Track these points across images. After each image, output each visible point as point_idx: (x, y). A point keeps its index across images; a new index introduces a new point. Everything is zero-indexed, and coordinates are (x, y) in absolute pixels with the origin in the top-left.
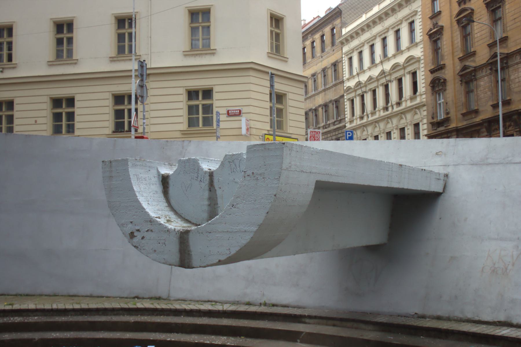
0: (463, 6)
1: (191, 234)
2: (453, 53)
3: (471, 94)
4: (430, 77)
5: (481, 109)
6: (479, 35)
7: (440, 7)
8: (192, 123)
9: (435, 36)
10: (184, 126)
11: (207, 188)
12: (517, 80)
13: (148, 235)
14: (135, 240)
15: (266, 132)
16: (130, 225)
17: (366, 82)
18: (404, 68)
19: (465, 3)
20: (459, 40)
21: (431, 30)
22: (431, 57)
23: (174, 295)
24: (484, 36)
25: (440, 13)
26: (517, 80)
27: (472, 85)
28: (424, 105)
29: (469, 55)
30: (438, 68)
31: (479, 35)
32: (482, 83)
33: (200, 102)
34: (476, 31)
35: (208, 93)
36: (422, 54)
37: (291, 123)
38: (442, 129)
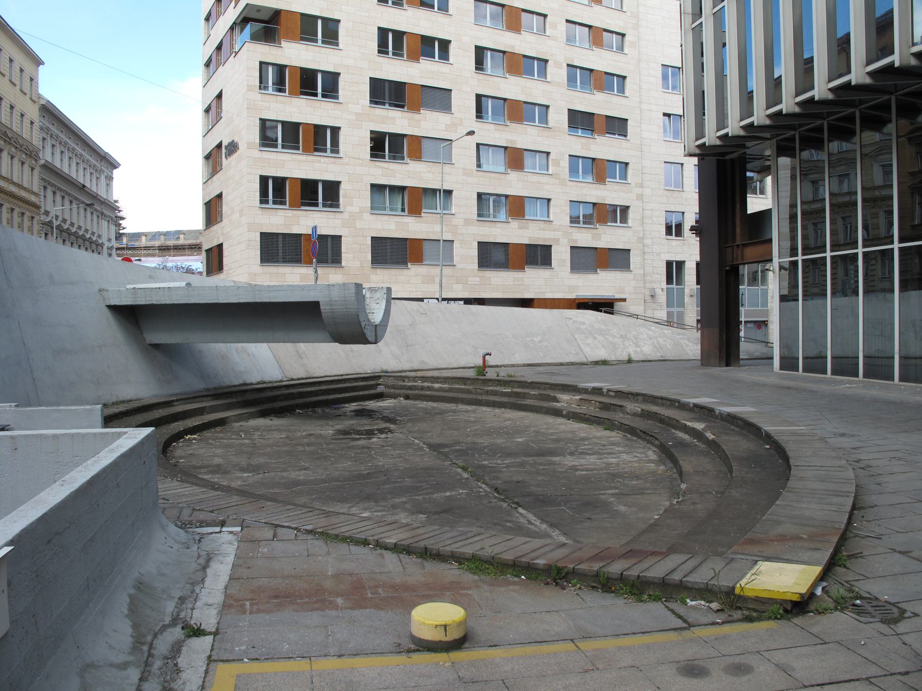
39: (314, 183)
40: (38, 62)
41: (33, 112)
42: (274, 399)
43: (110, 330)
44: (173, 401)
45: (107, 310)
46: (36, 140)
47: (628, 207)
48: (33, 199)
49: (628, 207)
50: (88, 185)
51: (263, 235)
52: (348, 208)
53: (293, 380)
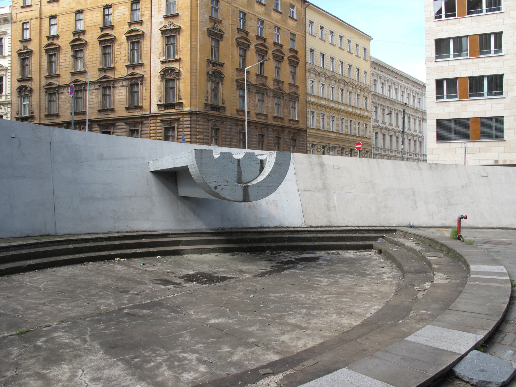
1: (249, 187)
2: (40, 71)
3: (52, 103)
4: (17, 85)
5: (61, 114)
6: (63, 64)
7: (30, 36)
9: (24, 56)
11: (237, 166)
13: (225, 188)
19: (53, 40)
20: (46, 63)
21: (21, 50)
22: (19, 70)
24: (67, 66)
25: (30, 40)
27: (54, 98)
28: (9, 104)
29: (51, 76)
30: (24, 79)
31: (63, 64)
32: (63, 97)
34: (61, 61)
36: (10, 65)
39: (480, 79)
40: (369, 38)
41: (366, 66)
42: (246, 241)
43: (154, 186)
44: (169, 234)
45: (151, 174)
46: (370, 81)
47: (501, 33)
48: (366, 114)
49: (501, 33)
50: (411, 103)
51: (438, 121)
52: (510, 94)
53: (311, 227)
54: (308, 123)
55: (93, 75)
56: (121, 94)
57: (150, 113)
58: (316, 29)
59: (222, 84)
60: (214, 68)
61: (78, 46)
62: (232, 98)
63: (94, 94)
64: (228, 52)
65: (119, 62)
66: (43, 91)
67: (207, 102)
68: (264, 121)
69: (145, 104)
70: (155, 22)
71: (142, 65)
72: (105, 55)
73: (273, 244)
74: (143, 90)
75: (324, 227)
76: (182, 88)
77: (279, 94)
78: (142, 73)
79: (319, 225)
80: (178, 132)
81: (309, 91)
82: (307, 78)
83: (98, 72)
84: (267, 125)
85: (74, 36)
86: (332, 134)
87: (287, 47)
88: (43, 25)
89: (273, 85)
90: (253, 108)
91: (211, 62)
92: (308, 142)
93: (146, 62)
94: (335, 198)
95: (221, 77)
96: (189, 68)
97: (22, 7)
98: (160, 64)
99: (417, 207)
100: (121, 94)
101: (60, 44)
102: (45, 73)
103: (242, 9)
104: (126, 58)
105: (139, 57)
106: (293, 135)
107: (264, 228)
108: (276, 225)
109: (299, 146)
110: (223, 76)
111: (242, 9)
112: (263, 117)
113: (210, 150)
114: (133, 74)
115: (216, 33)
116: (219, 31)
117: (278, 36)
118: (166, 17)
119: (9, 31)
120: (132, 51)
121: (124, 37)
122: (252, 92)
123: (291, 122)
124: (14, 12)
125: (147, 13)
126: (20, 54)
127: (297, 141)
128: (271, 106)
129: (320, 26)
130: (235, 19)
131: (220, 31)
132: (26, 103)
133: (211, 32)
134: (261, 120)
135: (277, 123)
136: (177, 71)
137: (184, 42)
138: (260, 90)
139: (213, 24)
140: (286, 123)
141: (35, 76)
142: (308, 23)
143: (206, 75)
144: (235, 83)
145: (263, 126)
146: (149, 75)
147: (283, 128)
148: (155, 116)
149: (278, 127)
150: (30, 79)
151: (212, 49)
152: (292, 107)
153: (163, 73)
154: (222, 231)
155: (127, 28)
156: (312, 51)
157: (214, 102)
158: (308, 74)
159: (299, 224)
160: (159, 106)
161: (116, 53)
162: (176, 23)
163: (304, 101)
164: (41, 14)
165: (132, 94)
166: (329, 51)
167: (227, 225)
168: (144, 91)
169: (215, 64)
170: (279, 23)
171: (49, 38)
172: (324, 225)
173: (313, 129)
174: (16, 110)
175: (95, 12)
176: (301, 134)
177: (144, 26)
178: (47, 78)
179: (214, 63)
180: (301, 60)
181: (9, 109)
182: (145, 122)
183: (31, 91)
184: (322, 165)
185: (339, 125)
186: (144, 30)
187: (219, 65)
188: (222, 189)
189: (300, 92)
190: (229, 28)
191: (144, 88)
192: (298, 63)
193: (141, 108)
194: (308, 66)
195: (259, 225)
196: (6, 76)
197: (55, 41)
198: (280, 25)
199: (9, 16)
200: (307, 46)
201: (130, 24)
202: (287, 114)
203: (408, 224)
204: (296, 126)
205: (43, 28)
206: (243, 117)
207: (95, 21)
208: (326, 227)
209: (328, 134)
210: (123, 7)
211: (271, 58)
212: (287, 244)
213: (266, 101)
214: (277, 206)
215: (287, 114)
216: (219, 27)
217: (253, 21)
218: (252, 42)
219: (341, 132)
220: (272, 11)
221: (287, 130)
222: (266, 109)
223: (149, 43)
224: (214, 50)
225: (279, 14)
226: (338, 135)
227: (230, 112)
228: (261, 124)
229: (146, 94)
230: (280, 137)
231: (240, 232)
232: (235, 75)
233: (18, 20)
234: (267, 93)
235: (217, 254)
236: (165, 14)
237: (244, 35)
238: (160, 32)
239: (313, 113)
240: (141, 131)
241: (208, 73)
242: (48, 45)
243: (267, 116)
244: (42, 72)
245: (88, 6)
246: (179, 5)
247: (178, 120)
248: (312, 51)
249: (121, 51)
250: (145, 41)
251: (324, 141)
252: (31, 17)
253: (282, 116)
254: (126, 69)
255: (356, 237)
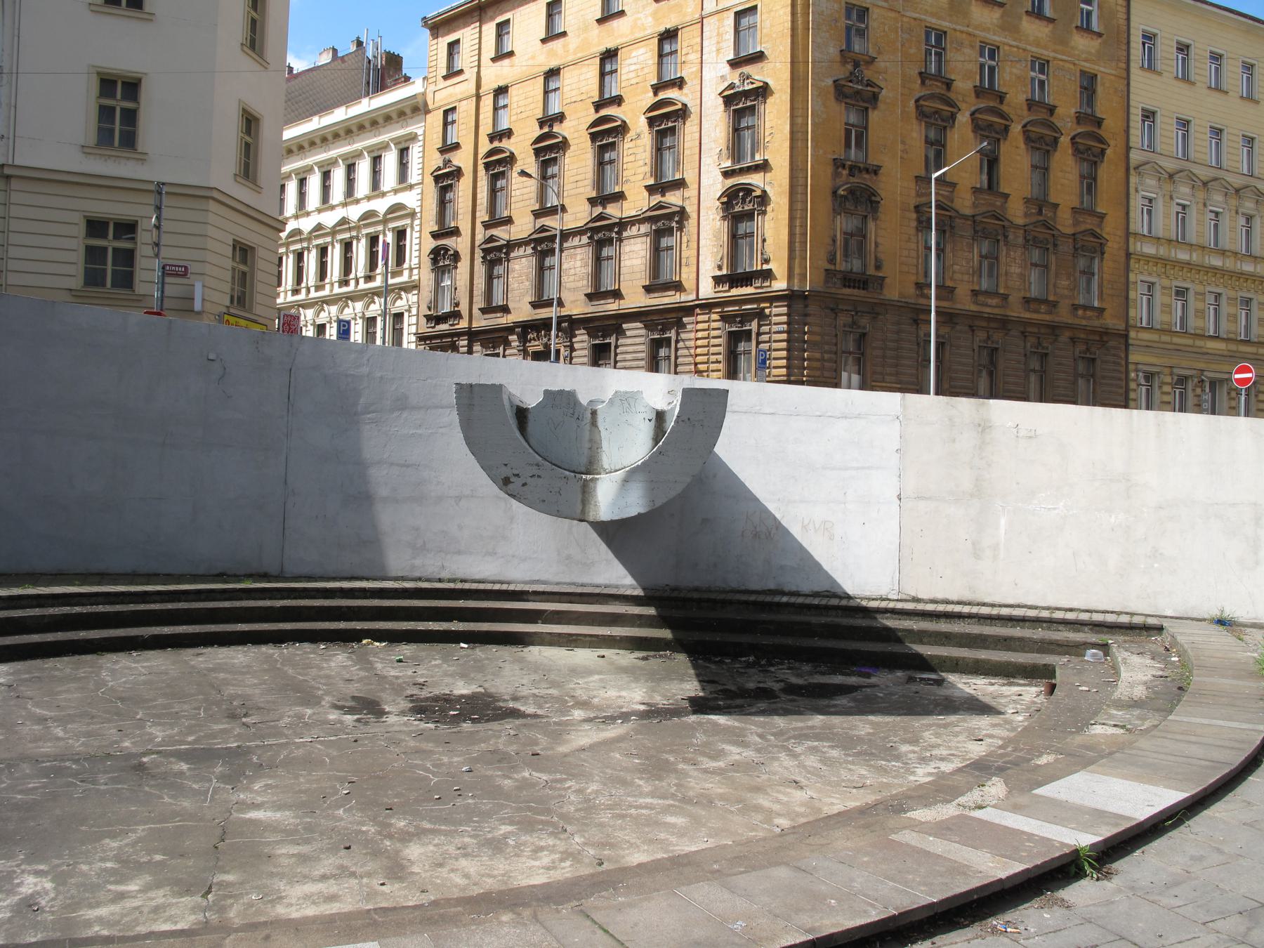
0: (496, 144)
4: (431, 244)
8: (93, 278)
9: (445, 180)
10: (77, 282)
12: (572, 271)
14: (511, 486)
15: (225, 310)
16: (504, 468)
17: (310, 233)
18: (385, 221)
19: (500, 141)
21: (439, 169)
23: (290, 569)
24: (526, 197)
26: (572, 271)
29: (496, 221)
30: (445, 231)
31: (518, 192)
32: (517, 267)
33: (110, 243)
35: (128, 228)
37: (643, 347)
38: (443, 327)
44: (527, 592)
53: (916, 600)
54: (1132, 313)
55: (578, 214)
56: (634, 254)
57: (698, 299)
58: (1166, 50)
59: (875, 219)
60: (852, 179)
61: (549, 150)
62: (905, 253)
63: (579, 257)
64: (895, 135)
65: (632, 179)
66: (479, 254)
67: (832, 267)
68: (996, 311)
69: (687, 277)
70: (708, 75)
71: (680, 184)
72: (601, 164)
73: (766, 641)
74: (682, 243)
75: (952, 603)
76: (769, 235)
77: (1042, 236)
78: (680, 203)
79: (940, 596)
80: (758, 343)
81: (1139, 223)
82: (1132, 190)
83: (587, 206)
84: (1004, 323)
85: (541, 128)
86: (1211, 345)
87: (1067, 109)
88: (481, 111)
89: (1026, 215)
90: (966, 277)
91: (844, 167)
92: (1131, 367)
93: (690, 176)
94: (1003, 521)
95: (871, 202)
96: (786, 182)
97: (445, 78)
98: (721, 178)
99: (1257, 563)
100: (634, 254)
101: (513, 150)
102: (483, 216)
103: (934, 21)
104: (647, 169)
105: (677, 163)
106: (1084, 347)
107: (783, 593)
108: (817, 589)
109: (1104, 377)
110: (878, 199)
111: (934, 21)
112: (994, 301)
113: (493, 385)
114: (660, 206)
115: (858, 92)
116: (868, 85)
117: (1042, 83)
118: (734, 64)
119: (420, 132)
120: (659, 150)
121: (643, 121)
122: (962, 236)
123: (1080, 312)
124: (432, 88)
125: (694, 57)
126: (437, 179)
127: (1098, 362)
128: (1018, 270)
129: (1178, 43)
130: (912, 51)
131: (870, 84)
132: (447, 282)
133: (845, 90)
134: (988, 310)
135: (1035, 316)
136: (758, 193)
137: (775, 119)
138: (989, 228)
139: (850, 67)
140: (1064, 315)
141: (464, 225)
142: (1136, 40)
143: (829, 198)
144: (914, 216)
145: (992, 325)
146: (696, 207)
147: (1054, 329)
148: (708, 306)
149: (1039, 325)
150: (455, 232)
151: (848, 133)
152: (1083, 272)
153: (725, 199)
154: (675, 594)
155: (649, 99)
156: (1149, 115)
157: (856, 265)
158: (1134, 179)
159: (883, 592)
160: (718, 280)
161: (625, 160)
162: (758, 74)
163: (1123, 254)
164: (478, 86)
165: (657, 252)
166: (1203, 107)
167: (690, 579)
168: (684, 246)
169: (854, 169)
170: (1045, 48)
171: (492, 138)
172: (955, 598)
173: (1150, 329)
174: (428, 300)
175: (584, 70)
176: (1112, 343)
177: (685, 90)
178: (487, 226)
179: (851, 168)
180: (1112, 143)
181: (415, 299)
182: (685, 320)
183: (456, 257)
184: (983, 427)
185: (1235, 316)
186: (685, 100)
187: (867, 171)
188: (524, 485)
189: (1110, 229)
190: (895, 75)
191: (685, 239)
192: (1103, 152)
193: (678, 287)
194: (1135, 157)
195: (772, 586)
196: (412, 228)
197: (505, 144)
198: (1047, 54)
199: (420, 99)
200: (1132, 103)
201: (656, 89)
202: (1066, 292)
203: (1215, 613)
204: (1096, 323)
205: (481, 117)
206: (922, 301)
207: (583, 90)
208: (959, 603)
209: (1199, 343)
210: (642, 51)
211: (1021, 139)
212: (818, 643)
213: (1003, 259)
214: (831, 538)
215: (1066, 292)
216: (868, 74)
217: (967, 51)
218: (962, 106)
219: (1211, 333)
220: (1025, 18)
221: (1067, 334)
222: (1002, 279)
223: (696, 128)
224: (857, 135)
225: (1045, 23)
226: (1233, 347)
227: (896, 289)
228: (989, 319)
229: (688, 253)
230: (1046, 354)
231: (709, 600)
232: (913, 193)
233: (437, 105)
234: (1006, 237)
235: (602, 652)
236: (731, 56)
237: (939, 88)
238: (720, 100)
239: (1151, 286)
240: (677, 342)
241: (835, 193)
242: (491, 153)
243: (1005, 297)
244: (478, 214)
245: (570, 58)
246: (764, 31)
247: (761, 315)
248: (1149, 115)
249: (636, 153)
250: (688, 123)
251: (1184, 364)
252: (460, 97)
253: (1051, 298)
254: (646, 194)
255: (1021, 639)
